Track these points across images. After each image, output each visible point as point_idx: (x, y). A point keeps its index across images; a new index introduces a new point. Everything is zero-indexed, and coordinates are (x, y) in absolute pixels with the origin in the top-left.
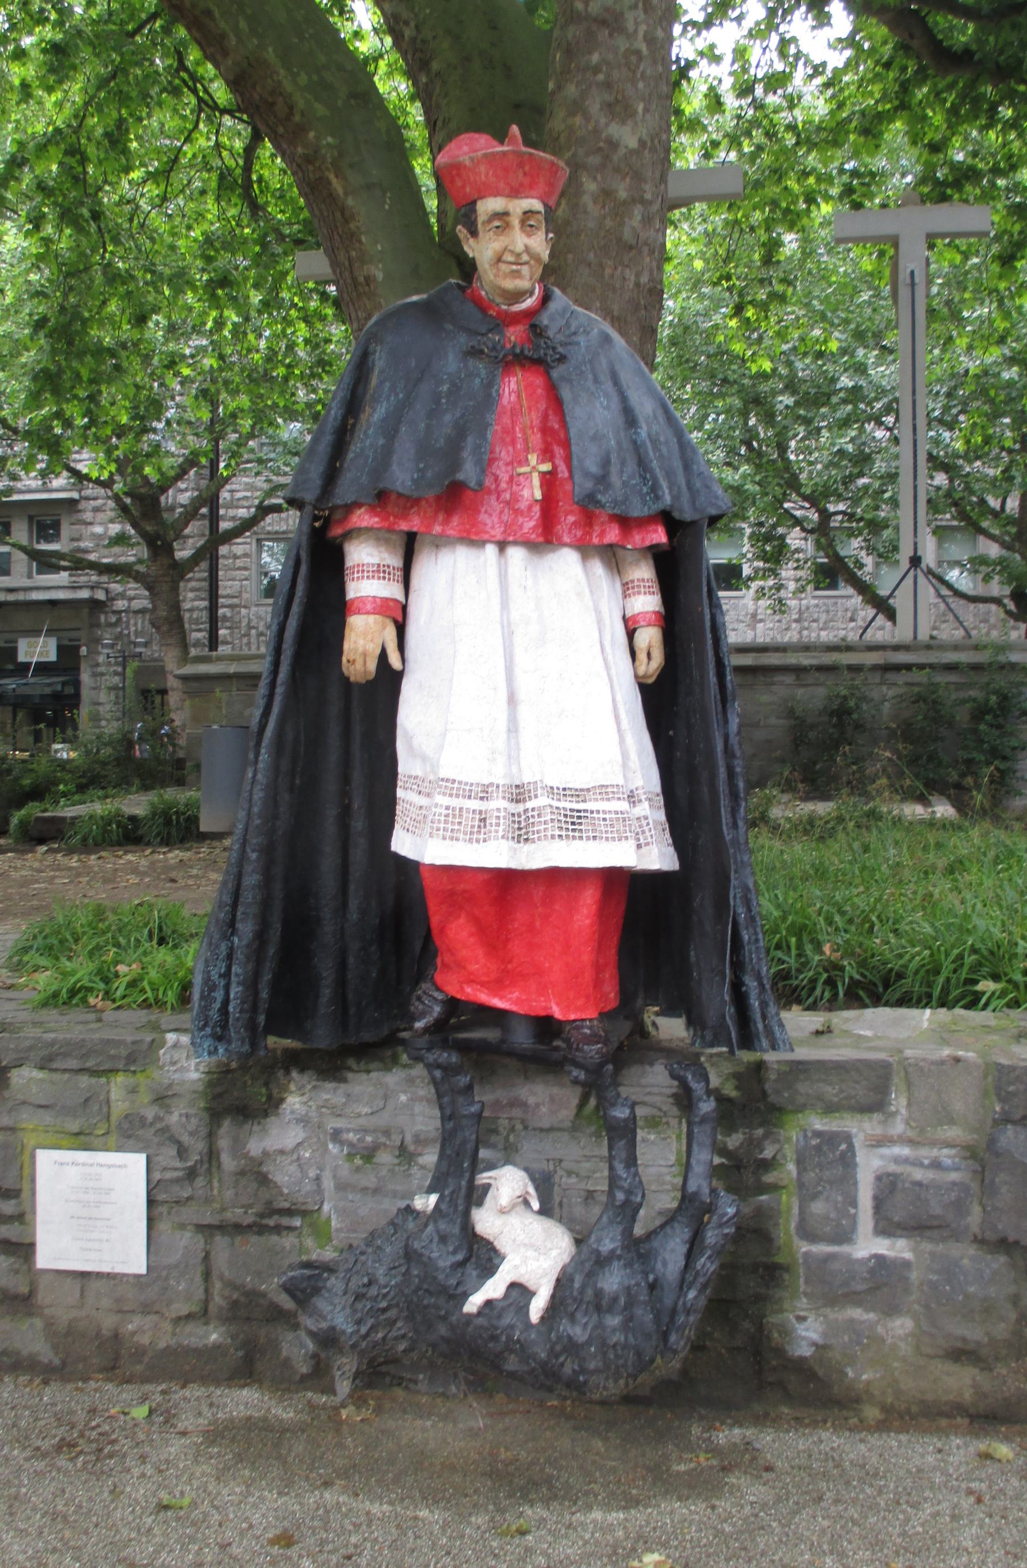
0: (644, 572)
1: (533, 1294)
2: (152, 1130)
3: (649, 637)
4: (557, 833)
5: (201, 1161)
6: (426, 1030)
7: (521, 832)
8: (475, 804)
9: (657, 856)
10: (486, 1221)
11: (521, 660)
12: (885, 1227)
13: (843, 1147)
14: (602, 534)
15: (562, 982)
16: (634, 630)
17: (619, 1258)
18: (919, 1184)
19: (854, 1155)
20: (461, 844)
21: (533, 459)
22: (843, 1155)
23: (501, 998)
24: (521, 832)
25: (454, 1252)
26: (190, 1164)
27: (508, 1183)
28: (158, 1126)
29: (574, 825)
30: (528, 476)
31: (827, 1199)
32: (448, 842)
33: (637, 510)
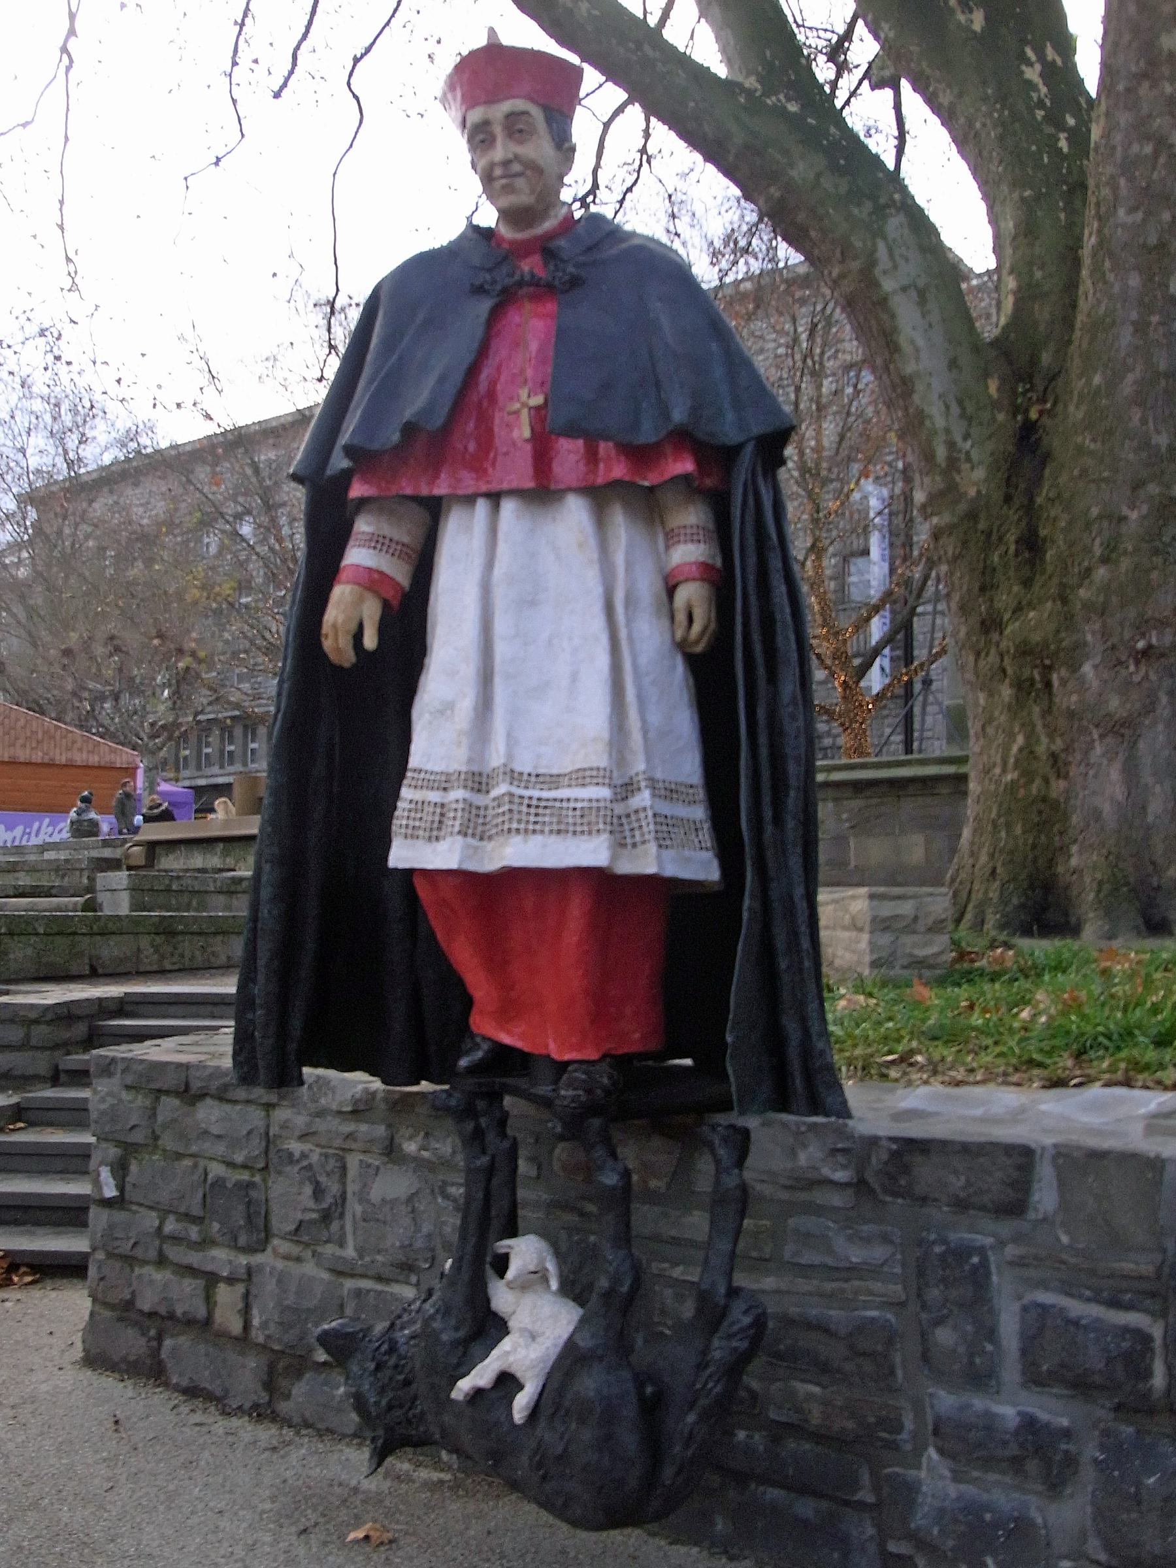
0: (692, 516)
1: (521, 1387)
2: (296, 1168)
3: (691, 593)
4: (531, 827)
5: (336, 1204)
6: (472, 1070)
7: (476, 825)
8: (434, 796)
9: (699, 865)
10: (502, 1297)
11: (502, 626)
12: (1034, 1378)
13: (975, 1260)
14: (609, 469)
15: (542, 1013)
16: (675, 587)
17: (601, 1359)
18: (1076, 1323)
19: (988, 1275)
20: (420, 843)
21: (524, 393)
22: (975, 1269)
23: (509, 1032)
24: (476, 825)
25: (457, 1329)
26: (325, 1205)
27: (525, 1252)
28: (305, 1163)
29: (535, 816)
30: (517, 413)
31: (955, 1328)
32: (409, 841)
33: (647, 434)
